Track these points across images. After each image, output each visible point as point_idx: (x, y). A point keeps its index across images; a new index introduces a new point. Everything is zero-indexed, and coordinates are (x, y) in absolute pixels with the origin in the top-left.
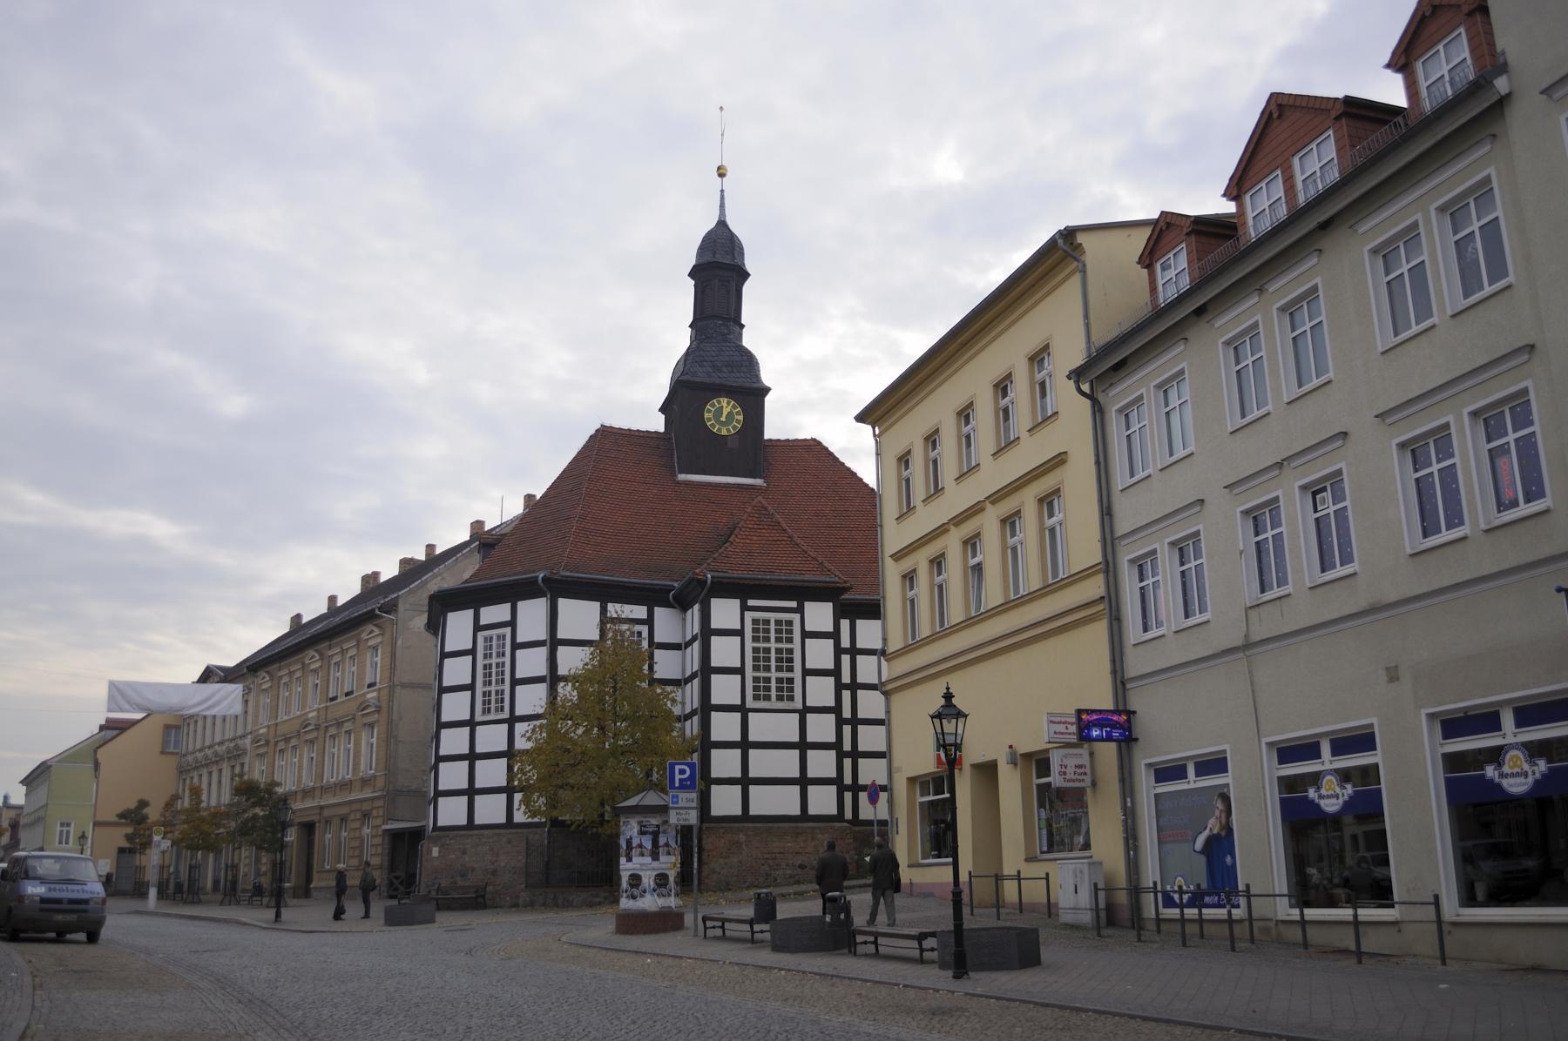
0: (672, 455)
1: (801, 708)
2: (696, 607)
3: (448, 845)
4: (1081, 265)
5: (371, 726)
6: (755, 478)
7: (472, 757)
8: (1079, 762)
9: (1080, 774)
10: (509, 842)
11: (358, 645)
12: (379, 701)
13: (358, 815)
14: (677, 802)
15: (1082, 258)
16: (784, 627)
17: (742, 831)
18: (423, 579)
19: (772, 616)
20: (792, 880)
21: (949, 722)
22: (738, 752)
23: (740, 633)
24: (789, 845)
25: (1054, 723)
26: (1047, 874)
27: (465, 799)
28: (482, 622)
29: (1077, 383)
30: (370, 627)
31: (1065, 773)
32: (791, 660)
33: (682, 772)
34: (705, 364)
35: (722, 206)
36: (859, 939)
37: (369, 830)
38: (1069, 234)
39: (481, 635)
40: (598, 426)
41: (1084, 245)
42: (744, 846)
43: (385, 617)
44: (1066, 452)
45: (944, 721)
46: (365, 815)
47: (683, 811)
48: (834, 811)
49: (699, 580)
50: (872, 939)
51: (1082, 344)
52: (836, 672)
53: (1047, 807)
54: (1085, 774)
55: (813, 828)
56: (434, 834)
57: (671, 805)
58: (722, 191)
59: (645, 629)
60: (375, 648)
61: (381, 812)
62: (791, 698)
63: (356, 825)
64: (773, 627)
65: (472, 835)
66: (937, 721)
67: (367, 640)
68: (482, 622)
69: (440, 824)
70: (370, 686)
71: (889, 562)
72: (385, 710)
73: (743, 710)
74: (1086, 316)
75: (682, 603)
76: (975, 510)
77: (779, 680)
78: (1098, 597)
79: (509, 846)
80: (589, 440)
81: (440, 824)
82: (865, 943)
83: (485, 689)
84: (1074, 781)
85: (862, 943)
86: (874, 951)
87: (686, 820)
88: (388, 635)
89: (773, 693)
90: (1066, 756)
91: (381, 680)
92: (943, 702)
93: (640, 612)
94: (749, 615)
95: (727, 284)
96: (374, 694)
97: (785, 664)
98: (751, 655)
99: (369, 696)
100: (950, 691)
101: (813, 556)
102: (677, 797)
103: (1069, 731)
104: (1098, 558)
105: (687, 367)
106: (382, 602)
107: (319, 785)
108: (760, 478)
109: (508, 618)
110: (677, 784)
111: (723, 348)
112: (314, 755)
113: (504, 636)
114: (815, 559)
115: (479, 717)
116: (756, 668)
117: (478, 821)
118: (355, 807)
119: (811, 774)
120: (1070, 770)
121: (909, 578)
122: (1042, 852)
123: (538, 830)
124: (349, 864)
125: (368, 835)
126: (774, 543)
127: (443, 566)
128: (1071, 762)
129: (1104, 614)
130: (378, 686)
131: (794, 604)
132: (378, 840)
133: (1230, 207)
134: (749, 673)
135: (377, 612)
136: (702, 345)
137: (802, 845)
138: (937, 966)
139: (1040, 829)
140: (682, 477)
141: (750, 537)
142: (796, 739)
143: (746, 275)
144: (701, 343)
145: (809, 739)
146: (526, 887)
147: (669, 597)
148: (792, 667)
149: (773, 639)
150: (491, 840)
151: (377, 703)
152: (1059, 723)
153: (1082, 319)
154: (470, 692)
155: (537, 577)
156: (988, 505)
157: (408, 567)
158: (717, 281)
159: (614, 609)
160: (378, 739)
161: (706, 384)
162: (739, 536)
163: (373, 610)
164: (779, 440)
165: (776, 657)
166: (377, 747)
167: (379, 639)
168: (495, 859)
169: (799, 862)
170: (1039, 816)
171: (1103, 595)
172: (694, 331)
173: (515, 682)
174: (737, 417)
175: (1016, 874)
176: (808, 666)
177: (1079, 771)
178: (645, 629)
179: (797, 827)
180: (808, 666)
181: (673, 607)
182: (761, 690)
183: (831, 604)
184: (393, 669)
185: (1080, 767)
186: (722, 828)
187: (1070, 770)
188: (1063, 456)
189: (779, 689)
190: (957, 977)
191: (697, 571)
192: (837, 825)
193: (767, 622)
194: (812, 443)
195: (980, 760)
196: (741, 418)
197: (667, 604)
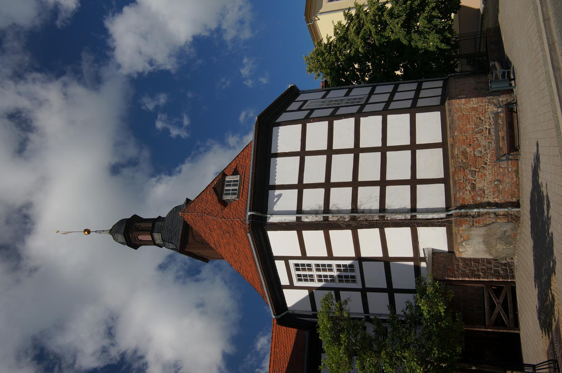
2: (277, 198)
39: (296, 283)
68: (288, 284)
93: (280, 266)
115: (359, 285)
133: (510, 82)
142: (409, 152)
145: (408, 143)
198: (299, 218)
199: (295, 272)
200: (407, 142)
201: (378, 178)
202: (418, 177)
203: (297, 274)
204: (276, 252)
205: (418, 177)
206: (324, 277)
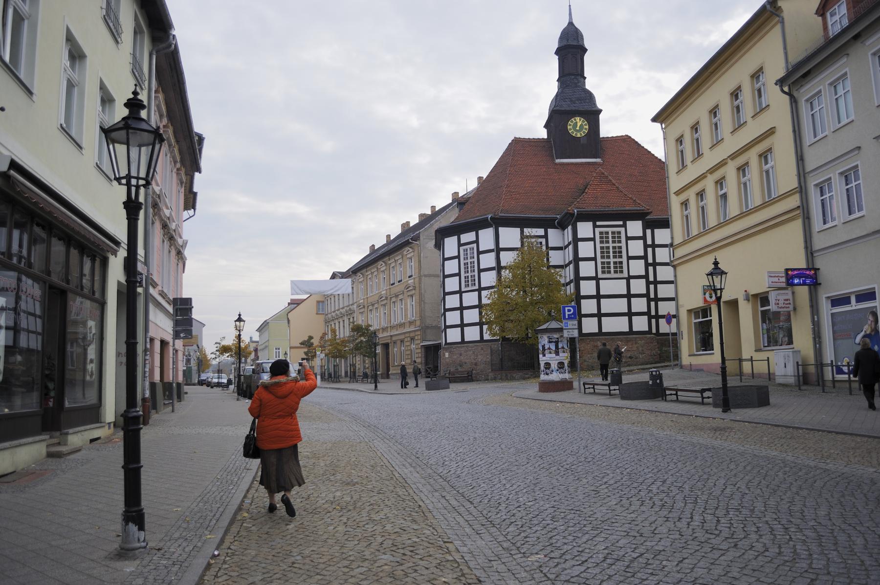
0: (552, 150)
1: (627, 276)
2: (570, 227)
5: (412, 296)
9: (787, 304)
10: (482, 349)
11: (402, 257)
13: (409, 339)
15: (782, 15)
19: (610, 230)
21: (717, 277)
23: (593, 239)
25: (772, 277)
26: (768, 358)
29: (781, 87)
30: (407, 248)
31: (778, 304)
33: (569, 311)
36: (668, 392)
39: (462, 248)
45: (714, 277)
47: (571, 331)
49: (570, 213)
53: (767, 322)
58: (570, 6)
59: (543, 241)
60: (411, 258)
61: (419, 337)
62: (622, 272)
64: (610, 235)
66: (710, 277)
72: (417, 289)
73: (596, 279)
74: (785, 48)
75: (562, 226)
78: (796, 206)
86: (676, 399)
87: (572, 335)
88: (416, 252)
89: (612, 270)
90: (778, 294)
92: (713, 266)
93: (541, 232)
94: (597, 230)
96: (412, 281)
99: (410, 282)
109: (474, 239)
110: (567, 317)
113: (473, 248)
114: (631, 198)
115: (463, 289)
116: (602, 257)
118: (407, 335)
120: (781, 302)
121: (685, 204)
128: (782, 298)
131: (621, 223)
132: (419, 351)
134: (599, 260)
135: (410, 241)
139: (763, 334)
140: (558, 161)
143: (585, 50)
148: (622, 256)
149: (611, 248)
155: (487, 218)
156: (729, 160)
157: (423, 218)
159: (527, 231)
163: (408, 240)
167: (412, 254)
171: (799, 205)
173: (480, 271)
176: (630, 255)
178: (543, 241)
181: (558, 228)
182: (606, 268)
185: (787, 300)
187: (781, 302)
188: (773, 130)
193: (607, 233)
194: (626, 137)
197: (554, 227)
198: (187, 198)
201: (625, 300)
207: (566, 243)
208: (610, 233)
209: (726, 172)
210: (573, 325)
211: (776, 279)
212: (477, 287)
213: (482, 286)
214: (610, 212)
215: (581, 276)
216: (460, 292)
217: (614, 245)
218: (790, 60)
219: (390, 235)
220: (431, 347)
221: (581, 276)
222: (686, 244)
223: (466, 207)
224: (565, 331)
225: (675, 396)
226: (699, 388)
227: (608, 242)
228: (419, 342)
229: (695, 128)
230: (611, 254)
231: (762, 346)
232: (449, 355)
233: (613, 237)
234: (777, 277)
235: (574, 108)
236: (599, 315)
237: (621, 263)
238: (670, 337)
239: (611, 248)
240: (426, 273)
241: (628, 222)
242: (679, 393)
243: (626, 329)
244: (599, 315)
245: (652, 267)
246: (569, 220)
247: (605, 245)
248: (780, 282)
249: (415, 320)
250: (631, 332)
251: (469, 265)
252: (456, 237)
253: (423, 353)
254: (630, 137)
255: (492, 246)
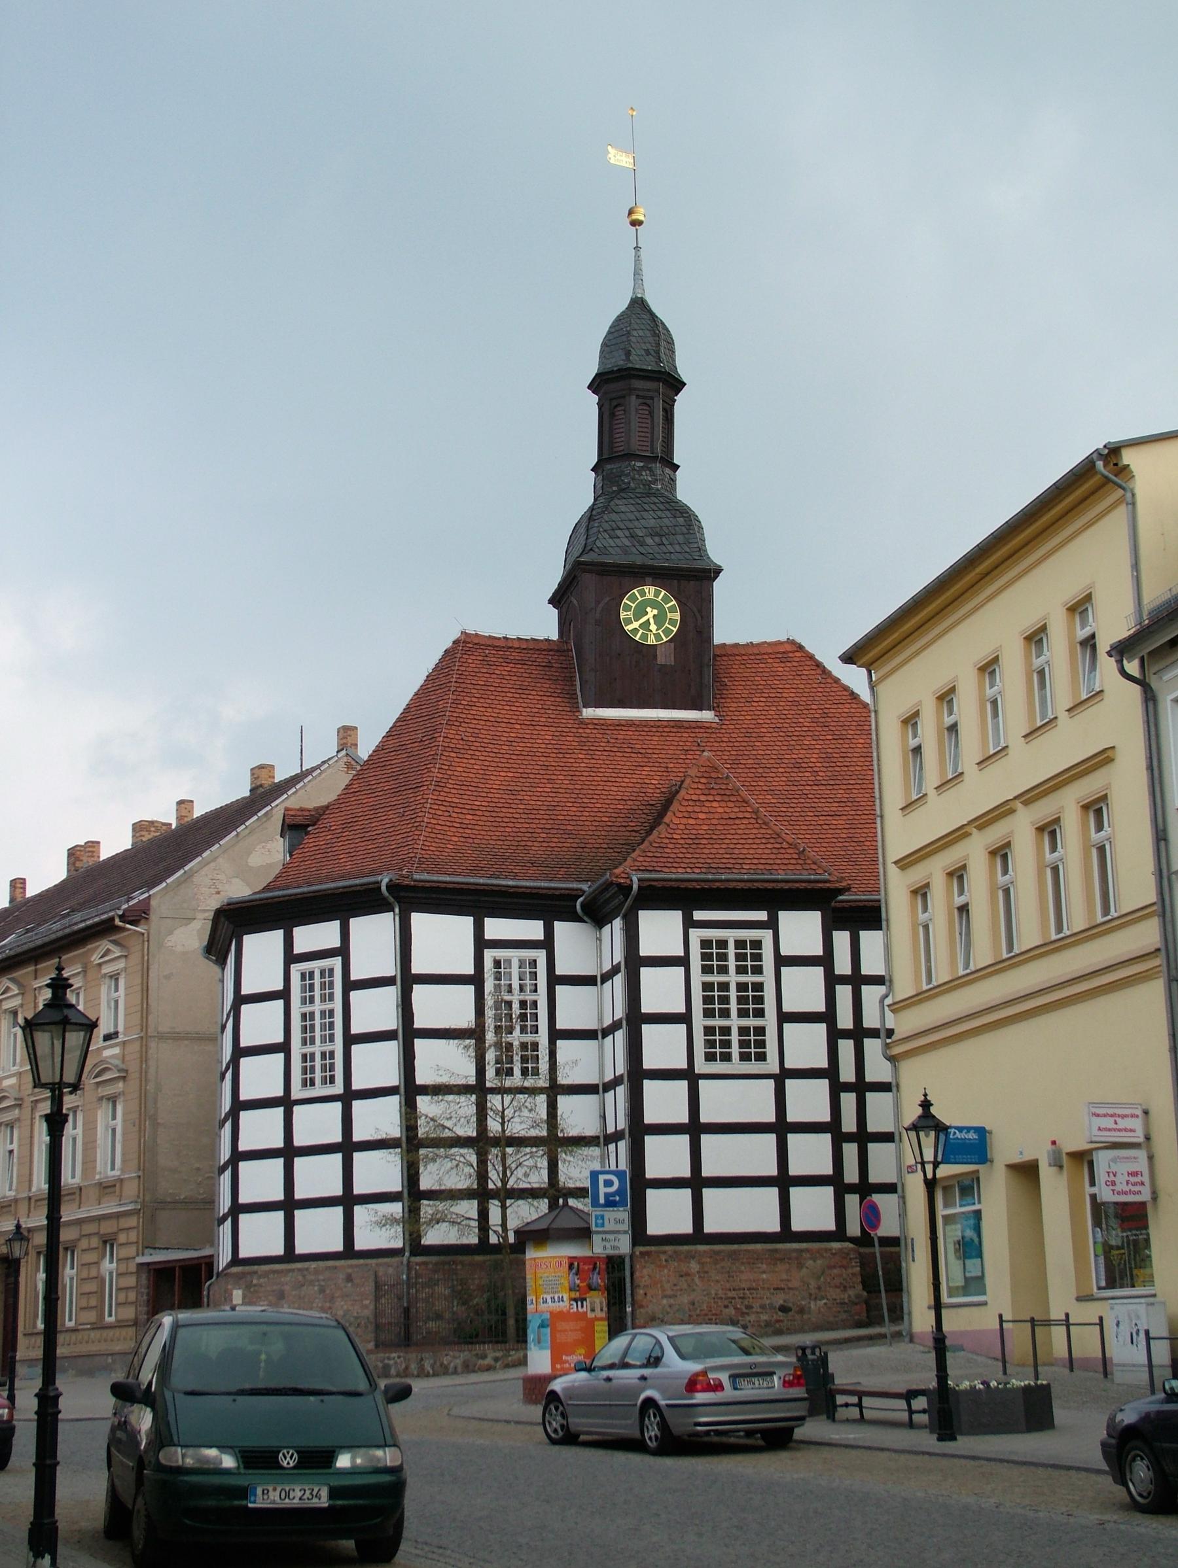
0: (572, 678)
1: (778, 1071)
2: (618, 923)
3: (255, 1285)
4: (1129, 495)
5: (113, 1100)
6: (701, 710)
7: (289, 1152)
8: (1133, 1167)
9: (1135, 1184)
10: (349, 1278)
11: (85, 971)
12: (123, 1061)
13: (95, 1242)
14: (603, 1225)
15: (1130, 485)
16: (749, 951)
17: (693, 1258)
18: (186, 868)
19: (731, 935)
20: (769, 1330)
21: (927, 1136)
22: (685, 1139)
23: (683, 961)
24: (764, 1276)
25: (1098, 1115)
26: (1101, 1319)
27: (280, 1215)
28: (298, 950)
29: (1120, 662)
30: (104, 944)
31: (1114, 1183)
32: (760, 1000)
33: (608, 1183)
34: (619, 533)
35: (637, 273)
36: (840, 1399)
37: (115, 1265)
38: (1112, 452)
39: (296, 969)
40: (456, 635)
41: (1131, 467)
42: (697, 1280)
43: (129, 929)
44: (1113, 747)
45: (922, 1134)
46: (105, 1242)
47: (611, 1237)
48: (831, 1226)
49: (619, 885)
50: (855, 1400)
51: (1129, 607)
52: (828, 1017)
53: (1104, 1226)
54: (1142, 1184)
55: (801, 1251)
56: (235, 1270)
57: (594, 1228)
58: (637, 248)
59: (541, 956)
60: (115, 977)
61: (133, 1236)
62: (761, 1057)
63: (91, 1257)
64: (731, 951)
65: (293, 1270)
66: (913, 1134)
67: (100, 965)
68: (298, 950)
69: (243, 1254)
70: (107, 1038)
71: (893, 870)
72: (134, 1076)
73: (690, 1076)
74: (1136, 566)
75: (597, 915)
76: (1002, 812)
77: (743, 1031)
78: (1153, 950)
79: (350, 1285)
80: (444, 657)
81: (243, 1254)
82: (847, 1405)
83: (304, 1051)
84: (1126, 1193)
85: (841, 1406)
86: (858, 1416)
87: (614, 1248)
88: (135, 958)
89: (735, 1050)
90: (1114, 1160)
91: (125, 1028)
92: (920, 1111)
93: (533, 929)
94: (696, 935)
95: (648, 402)
96: (116, 1051)
97: (751, 1006)
98: (701, 993)
99: (107, 1053)
100: (928, 1098)
101: (791, 841)
102: (602, 1217)
103: (1117, 1127)
104: (1152, 897)
105: (589, 541)
106: (125, 906)
107: (25, 1195)
108: (709, 709)
109: (336, 943)
110: (602, 1201)
111: (646, 506)
112: (15, 1146)
113: (331, 971)
114: (793, 846)
115: (297, 1093)
116: (708, 1013)
117: (301, 1248)
118: (90, 1228)
119: (794, 1170)
120: (1121, 1179)
121: (921, 892)
122: (1099, 1288)
123: (394, 1260)
124: (82, 1320)
125: (111, 1273)
126: (731, 822)
127: (217, 846)
128: (1123, 1169)
129: (1160, 972)
130: (121, 1038)
131: (762, 916)
132: (131, 1281)
134: (699, 1021)
135: (117, 922)
136: (612, 503)
137: (784, 1276)
138: (928, 1430)
139: (1096, 1256)
140: (588, 713)
141: (693, 815)
143: (677, 385)
144: (612, 499)
146: (377, 1346)
147: (575, 906)
148: (763, 1010)
149: (733, 987)
150: (321, 1277)
151: (122, 1066)
152: (1105, 1116)
153: (1130, 569)
154: (282, 1055)
155: (379, 883)
156: (1018, 805)
157: (147, 837)
158: (633, 398)
159: (496, 928)
160: (124, 1121)
161: (619, 565)
162: (678, 814)
163: (112, 919)
164: (736, 645)
165: (738, 997)
166: (124, 1134)
167: (121, 964)
168: (328, 1305)
169: (781, 1302)
170: (1094, 1237)
171: (1158, 945)
172: (600, 477)
173: (351, 1040)
174: (669, 615)
175: (1064, 1318)
176: (786, 1008)
177: (1133, 1179)
178: (541, 956)
179: (776, 1251)
180: (786, 1008)
181: (584, 921)
182: (718, 1047)
183: (819, 913)
184: (145, 1010)
185: (1134, 1174)
186: (665, 1252)
187: (1121, 1179)
188: (1109, 753)
189: (743, 1044)
190: (940, 1439)
191: (617, 871)
192: (836, 1245)
193: (723, 944)
194: (789, 648)
195: (1017, 1159)
196: (677, 616)
197: (574, 917)
199: (319, 968)
200: (686, 1194)
202: (868, 1079)
203: (313, 972)
204: (357, 924)
205: (868, 1079)
206: (310, 1025)
207: (607, 967)
208: (731, 945)
209: (1012, 832)
210: (617, 1221)
211: (1108, 1123)
212: (338, 1088)
213: (356, 1086)
214: (732, 885)
215: (645, 1067)
216: (286, 1102)
217: (743, 978)
218: (1146, 600)
219: (23, 881)
220: (173, 1269)
221: (645, 1067)
222: (921, 1001)
223: (310, 842)
224: (596, 1238)
225: (857, 1409)
226: (902, 1388)
227: (724, 970)
228: (131, 1251)
229: (946, 697)
230: (734, 1006)
231: (1095, 1290)
232: (244, 1297)
233: (739, 957)
234: (1112, 1116)
235: (639, 560)
236: (697, 1183)
237: (761, 1031)
238: (877, 1249)
239: (733, 987)
240: (164, 1027)
241: (782, 915)
242: (866, 1401)
243: (772, 1225)
244: (697, 1183)
245: (850, 1043)
246: (616, 902)
247: (715, 978)
248: (1120, 1130)
249: (122, 1180)
250: (786, 1233)
251: (317, 1022)
252: (280, 933)
253: (145, 1291)
254: (800, 648)
255: (389, 968)
